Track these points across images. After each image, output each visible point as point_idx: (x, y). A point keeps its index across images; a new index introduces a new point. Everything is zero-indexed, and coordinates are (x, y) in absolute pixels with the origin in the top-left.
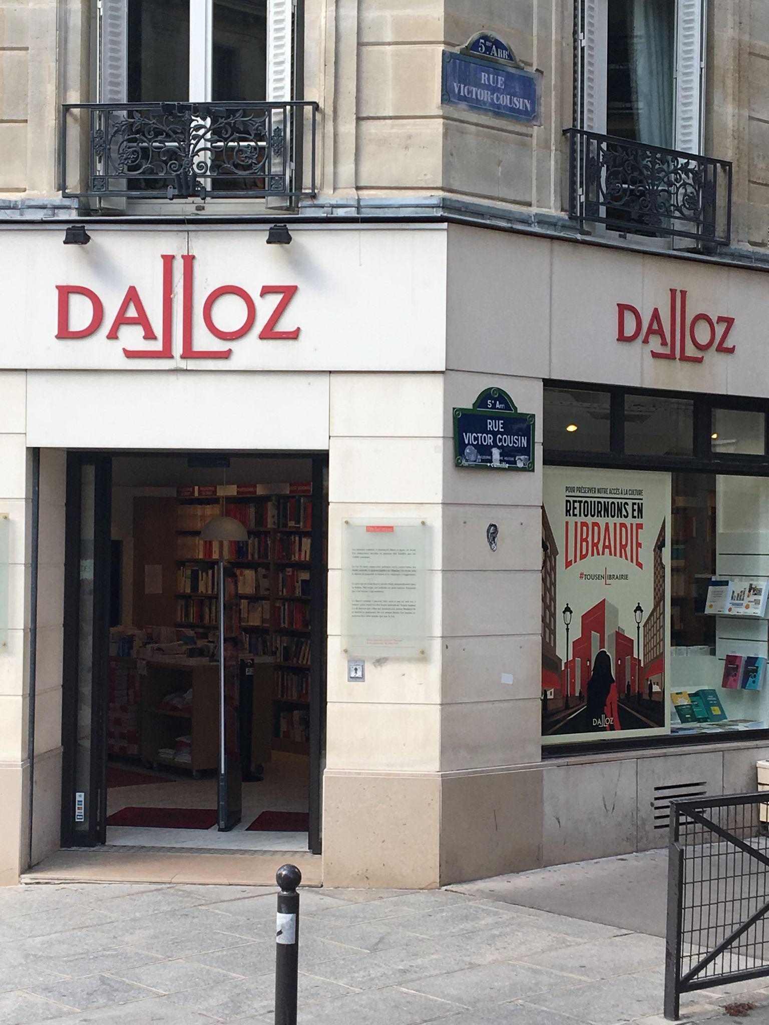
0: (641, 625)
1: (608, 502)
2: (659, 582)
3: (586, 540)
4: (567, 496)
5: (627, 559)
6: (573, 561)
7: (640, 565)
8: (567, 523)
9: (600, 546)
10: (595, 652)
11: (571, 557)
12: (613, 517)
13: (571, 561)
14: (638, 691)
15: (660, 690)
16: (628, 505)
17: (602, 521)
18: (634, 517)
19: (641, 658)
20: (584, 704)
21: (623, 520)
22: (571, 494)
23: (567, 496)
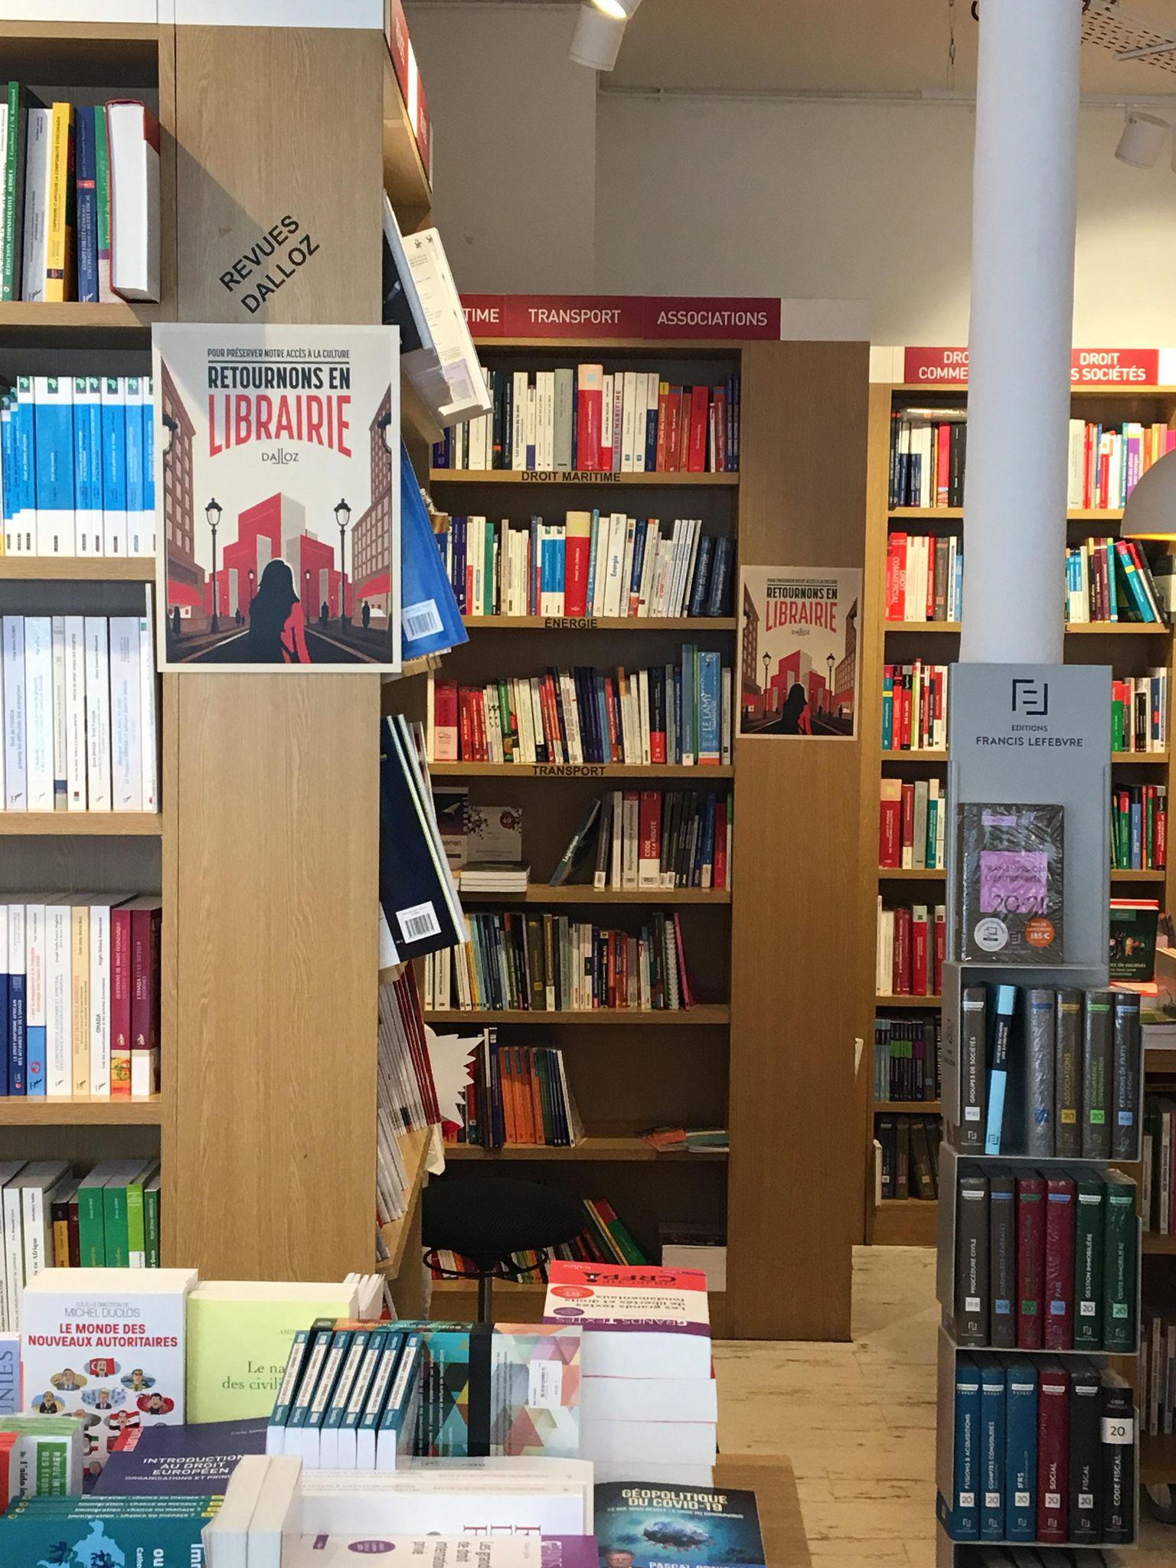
0: (348, 529)
1: (285, 369)
5: (321, 442)
7: (347, 452)
9: (798, 617)
11: (771, 623)
14: (343, 615)
17: (800, 601)
18: (332, 387)
19: (348, 570)
21: (313, 392)
22: (216, 359)
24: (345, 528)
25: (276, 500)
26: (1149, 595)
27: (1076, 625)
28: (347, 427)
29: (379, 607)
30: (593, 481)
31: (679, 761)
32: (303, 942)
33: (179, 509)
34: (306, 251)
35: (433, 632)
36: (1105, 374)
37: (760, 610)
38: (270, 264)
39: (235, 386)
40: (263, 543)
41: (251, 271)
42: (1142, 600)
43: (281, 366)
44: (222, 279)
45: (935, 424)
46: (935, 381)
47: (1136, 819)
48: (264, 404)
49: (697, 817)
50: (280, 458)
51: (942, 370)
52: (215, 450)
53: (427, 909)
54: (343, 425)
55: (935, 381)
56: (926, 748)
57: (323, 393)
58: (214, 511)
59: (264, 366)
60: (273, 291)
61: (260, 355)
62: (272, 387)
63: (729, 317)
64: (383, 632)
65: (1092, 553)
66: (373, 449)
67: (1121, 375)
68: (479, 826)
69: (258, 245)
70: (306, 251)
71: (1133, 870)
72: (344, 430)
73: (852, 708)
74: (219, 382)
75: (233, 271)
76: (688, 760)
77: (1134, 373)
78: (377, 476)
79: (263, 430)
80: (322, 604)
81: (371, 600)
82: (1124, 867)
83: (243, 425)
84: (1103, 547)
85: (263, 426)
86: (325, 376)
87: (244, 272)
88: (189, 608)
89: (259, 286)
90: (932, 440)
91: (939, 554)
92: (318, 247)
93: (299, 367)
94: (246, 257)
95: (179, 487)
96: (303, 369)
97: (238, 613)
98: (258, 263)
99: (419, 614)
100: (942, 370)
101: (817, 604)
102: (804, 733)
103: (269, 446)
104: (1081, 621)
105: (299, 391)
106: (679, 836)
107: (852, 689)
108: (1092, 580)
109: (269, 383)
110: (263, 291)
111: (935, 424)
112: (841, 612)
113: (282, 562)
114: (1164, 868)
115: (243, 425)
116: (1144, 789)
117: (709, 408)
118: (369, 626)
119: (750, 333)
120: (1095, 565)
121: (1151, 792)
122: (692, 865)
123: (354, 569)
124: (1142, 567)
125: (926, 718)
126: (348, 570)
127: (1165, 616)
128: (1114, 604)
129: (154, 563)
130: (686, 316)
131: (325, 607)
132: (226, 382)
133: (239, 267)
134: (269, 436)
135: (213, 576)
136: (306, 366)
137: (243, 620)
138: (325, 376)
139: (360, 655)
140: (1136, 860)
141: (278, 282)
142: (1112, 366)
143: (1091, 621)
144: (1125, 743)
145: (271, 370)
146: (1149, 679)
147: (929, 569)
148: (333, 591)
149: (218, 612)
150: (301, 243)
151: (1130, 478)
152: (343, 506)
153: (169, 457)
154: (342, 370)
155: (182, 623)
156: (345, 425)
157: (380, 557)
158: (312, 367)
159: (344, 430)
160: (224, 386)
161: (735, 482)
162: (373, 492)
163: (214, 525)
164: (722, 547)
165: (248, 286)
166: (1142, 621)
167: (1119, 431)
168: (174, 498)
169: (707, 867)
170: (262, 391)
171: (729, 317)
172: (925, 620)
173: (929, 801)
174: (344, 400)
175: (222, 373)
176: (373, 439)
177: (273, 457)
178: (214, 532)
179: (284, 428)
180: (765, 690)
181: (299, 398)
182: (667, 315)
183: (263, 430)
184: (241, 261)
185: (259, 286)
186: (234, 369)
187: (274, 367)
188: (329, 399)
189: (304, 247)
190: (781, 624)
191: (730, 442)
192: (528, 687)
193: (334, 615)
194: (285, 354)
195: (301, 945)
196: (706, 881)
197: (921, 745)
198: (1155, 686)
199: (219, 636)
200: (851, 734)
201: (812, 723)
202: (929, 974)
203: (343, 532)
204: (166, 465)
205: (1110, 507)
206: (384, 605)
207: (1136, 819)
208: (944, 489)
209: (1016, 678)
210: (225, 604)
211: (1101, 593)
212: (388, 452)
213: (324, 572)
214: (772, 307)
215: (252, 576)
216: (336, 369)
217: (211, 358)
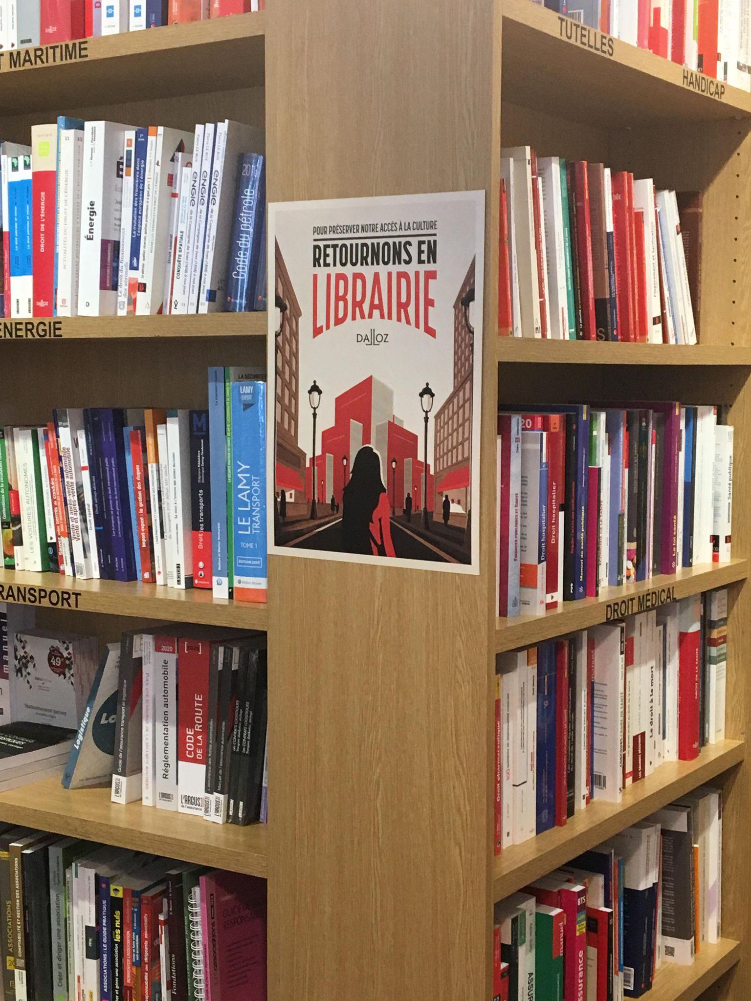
0: (431, 416)
4: (315, 240)
5: (408, 322)
6: (324, 328)
7: (431, 332)
9: (366, 306)
11: (322, 322)
14: (425, 508)
15: (464, 512)
17: (368, 271)
18: (420, 261)
20: (337, 516)
21: (403, 268)
23: (315, 240)
24: (429, 415)
28: (433, 305)
29: (459, 503)
30: (51, 63)
33: (287, 392)
39: (335, 265)
54: (429, 303)
58: (316, 394)
64: (460, 530)
66: (456, 330)
68: (26, 667)
72: (430, 308)
73: (465, 502)
74: (322, 261)
76: (220, 592)
78: (459, 358)
79: (357, 309)
80: (406, 496)
97: (333, 500)
105: (391, 267)
113: (372, 449)
123: (436, 459)
126: (431, 461)
131: (409, 499)
136: (397, 240)
137: (338, 507)
139: (442, 554)
148: (416, 483)
149: (316, 499)
153: (280, 339)
154: (429, 242)
158: (403, 240)
159: (430, 308)
160: (327, 265)
162: (455, 376)
168: (283, 380)
174: (431, 275)
176: (456, 317)
178: (315, 415)
181: (390, 274)
186: (335, 247)
188: (417, 274)
190: (338, 322)
192: (30, 443)
199: (317, 522)
203: (426, 419)
209: (170, 158)
210: (323, 488)
213: (408, 461)
215: (345, 461)
216: (424, 242)
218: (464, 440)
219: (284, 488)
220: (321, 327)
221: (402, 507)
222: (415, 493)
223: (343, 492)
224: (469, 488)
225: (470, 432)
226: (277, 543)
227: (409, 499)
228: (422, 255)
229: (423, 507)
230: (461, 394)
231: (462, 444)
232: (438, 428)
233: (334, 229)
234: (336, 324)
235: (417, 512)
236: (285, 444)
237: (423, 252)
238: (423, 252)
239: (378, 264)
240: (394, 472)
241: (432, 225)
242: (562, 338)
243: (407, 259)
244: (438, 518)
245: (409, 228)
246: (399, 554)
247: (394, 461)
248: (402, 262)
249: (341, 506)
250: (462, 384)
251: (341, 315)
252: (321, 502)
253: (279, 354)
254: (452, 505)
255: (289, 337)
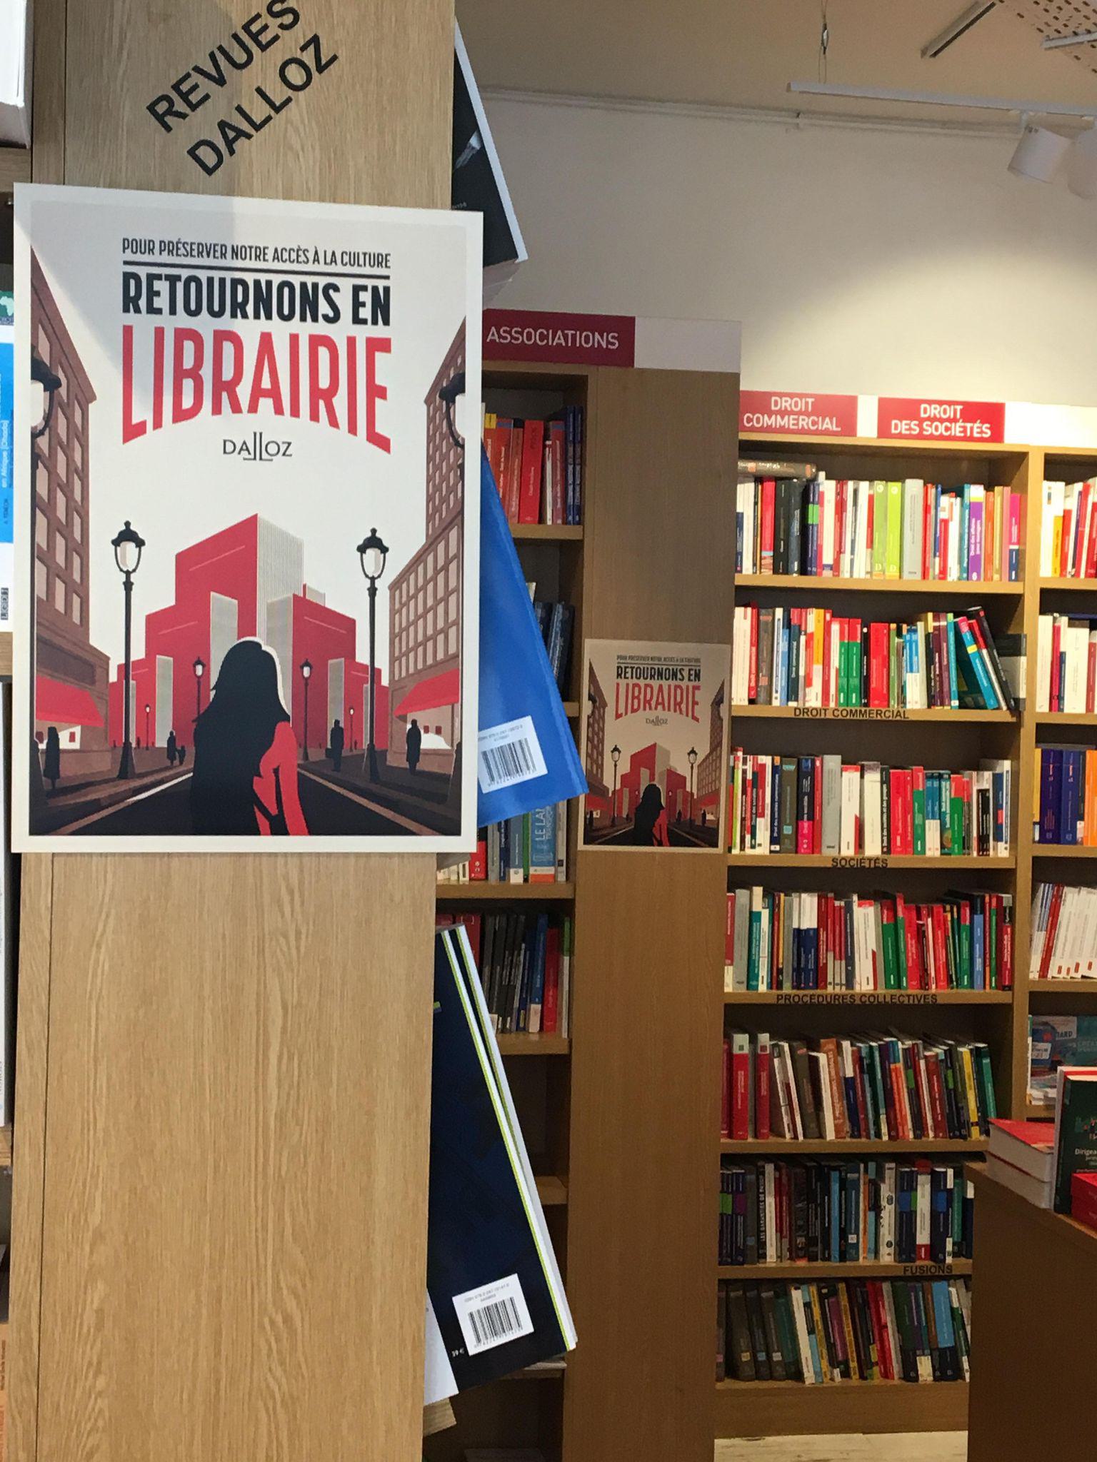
0: (382, 586)
1: (269, 283)
2: (445, 478)
3: (638, 698)
4: (126, 263)
5: (334, 422)
6: (150, 425)
7: (383, 443)
8: (618, 684)
9: (653, 703)
10: (222, 641)
11: (621, 710)
12: (287, 318)
13: (143, 424)
14: (371, 746)
15: (449, 748)
16: (308, 251)
17: (655, 683)
18: (357, 320)
19: (382, 662)
20: (182, 769)
21: (322, 328)
22: (139, 257)
23: (126, 263)
24: (378, 583)
25: (247, 530)
26: (993, 677)
27: (913, 711)
29: (438, 731)
31: (504, 877)
32: (282, 1363)
33: (60, 542)
34: (312, 64)
35: (528, 776)
36: (947, 429)
37: (609, 696)
38: (244, 84)
39: (173, 311)
40: (223, 607)
41: (207, 97)
42: (986, 684)
43: (263, 278)
44: (151, 108)
45: (759, 479)
46: (761, 430)
47: (978, 932)
48: (228, 348)
49: (523, 945)
50: (257, 450)
51: (770, 417)
52: (132, 431)
53: (509, 1288)
55: (761, 430)
56: (748, 851)
57: (340, 332)
58: (130, 547)
59: (229, 276)
60: (249, 136)
61: (223, 255)
62: (245, 316)
63: (574, 336)
64: (443, 778)
65: (931, 630)
66: (430, 439)
67: (965, 431)
69: (221, 48)
70: (312, 64)
71: (975, 991)
72: (378, 401)
74: (143, 303)
75: (174, 95)
77: (980, 429)
78: (438, 488)
79: (225, 395)
80: (331, 725)
81: (423, 717)
82: (964, 987)
83: (188, 385)
84: (943, 623)
85: (226, 389)
86: (344, 300)
87: (194, 98)
88: (77, 730)
89: (223, 125)
90: (756, 496)
91: (762, 626)
92: (334, 58)
93: (296, 280)
94: (197, 69)
95: (61, 499)
96: (304, 285)
98: (221, 81)
99: (504, 742)
100: (770, 417)
101: (676, 687)
102: (660, 844)
103: (240, 427)
104: (918, 706)
105: (295, 325)
106: (502, 969)
107: (717, 792)
108: (930, 661)
109: (238, 309)
110: (232, 135)
111: (759, 479)
112: (705, 698)
113: (259, 645)
114: (1010, 988)
115: (188, 385)
116: (987, 899)
117: (545, 446)
118: (419, 767)
119: (601, 357)
120: (933, 644)
121: (994, 901)
122: (516, 1004)
123: (393, 660)
124: (987, 647)
125: (748, 815)
126: (382, 662)
127: (1012, 703)
128: (954, 688)
129: (10, 643)
130: (521, 333)
131: (337, 731)
132: (158, 302)
133: (185, 87)
134: (236, 408)
135: (125, 669)
136: (309, 280)
138: (344, 300)
139: (699, 842)
140: (978, 980)
141: (258, 121)
142: (954, 420)
143: (929, 707)
144: (966, 845)
145: (244, 283)
146: (991, 773)
147: (752, 645)
148: (352, 700)
149: (133, 740)
150: (303, 49)
151: (972, 547)
152: (373, 542)
153: (43, 442)
154: (375, 289)
155: (63, 758)
156: (382, 392)
157: (441, 638)
158: (322, 281)
159: (378, 401)
160: (152, 310)
161: (579, 537)
162: (430, 518)
163: (128, 573)
164: (559, 614)
165: (202, 125)
166: (984, 707)
167: (960, 494)
169: (535, 1008)
170: (226, 323)
171: (574, 336)
172: (746, 703)
173: (751, 913)
174: (378, 345)
175: (150, 286)
176: (431, 420)
177: (245, 447)
179: (266, 394)
180: (614, 792)
182: (498, 332)
183: (225, 395)
184: (188, 76)
185: (223, 125)
186: (173, 280)
187: (250, 278)
188: (351, 342)
189: (308, 57)
190: (634, 711)
191: (571, 488)
193: (685, 817)
194: (270, 256)
195: (279, 1372)
196: (534, 1025)
197: (742, 848)
198: (997, 779)
200: (716, 845)
201: (670, 832)
202: (750, 1114)
203: (373, 591)
204: (36, 457)
205: (949, 579)
206: (446, 729)
207: (978, 932)
208: (768, 554)
210: (148, 723)
211: (941, 675)
212: (459, 444)
213: (336, 665)
214: (624, 327)
216: (364, 288)
217: (129, 256)
218: (448, 625)
219: (54, 724)
220: (143, 424)
221: (322, 745)
222: (684, 809)
223: (194, 726)
224: (458, 706)
225: (720, 774)
226: (585, 843)
227: (680, 813)
228: (361, 310)
229: (688, 817)
230: (441, 547)
231: (445, 631)
232: (397, 606)
233: (631, 658)
234: (632, 712)
235: (355, 752)
236: (58, 641)
237: (363, 305)
238: (363, 305)
239: (662, 679)
240: (306, 684)
241: (697, 660)
242: (848, 851)
243: (331, 314)
244: (397, 759)
245: (334, 261)
246: (672, 845)
247: (307, 664)
248: (320, 318)
249: (191, 752)
250: (444, 530)
251: (636, 707)
252: (143, 745)
253: (590, 729)
254: (424, 737)
255: (64, 439)
